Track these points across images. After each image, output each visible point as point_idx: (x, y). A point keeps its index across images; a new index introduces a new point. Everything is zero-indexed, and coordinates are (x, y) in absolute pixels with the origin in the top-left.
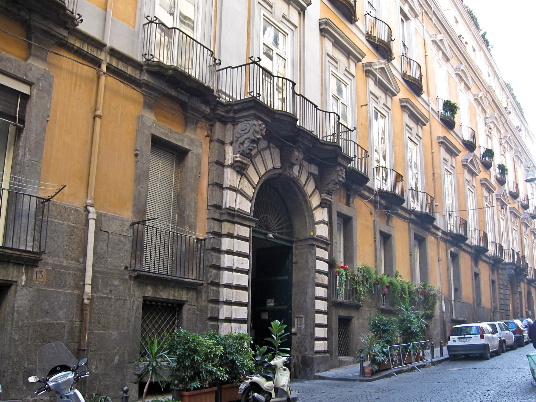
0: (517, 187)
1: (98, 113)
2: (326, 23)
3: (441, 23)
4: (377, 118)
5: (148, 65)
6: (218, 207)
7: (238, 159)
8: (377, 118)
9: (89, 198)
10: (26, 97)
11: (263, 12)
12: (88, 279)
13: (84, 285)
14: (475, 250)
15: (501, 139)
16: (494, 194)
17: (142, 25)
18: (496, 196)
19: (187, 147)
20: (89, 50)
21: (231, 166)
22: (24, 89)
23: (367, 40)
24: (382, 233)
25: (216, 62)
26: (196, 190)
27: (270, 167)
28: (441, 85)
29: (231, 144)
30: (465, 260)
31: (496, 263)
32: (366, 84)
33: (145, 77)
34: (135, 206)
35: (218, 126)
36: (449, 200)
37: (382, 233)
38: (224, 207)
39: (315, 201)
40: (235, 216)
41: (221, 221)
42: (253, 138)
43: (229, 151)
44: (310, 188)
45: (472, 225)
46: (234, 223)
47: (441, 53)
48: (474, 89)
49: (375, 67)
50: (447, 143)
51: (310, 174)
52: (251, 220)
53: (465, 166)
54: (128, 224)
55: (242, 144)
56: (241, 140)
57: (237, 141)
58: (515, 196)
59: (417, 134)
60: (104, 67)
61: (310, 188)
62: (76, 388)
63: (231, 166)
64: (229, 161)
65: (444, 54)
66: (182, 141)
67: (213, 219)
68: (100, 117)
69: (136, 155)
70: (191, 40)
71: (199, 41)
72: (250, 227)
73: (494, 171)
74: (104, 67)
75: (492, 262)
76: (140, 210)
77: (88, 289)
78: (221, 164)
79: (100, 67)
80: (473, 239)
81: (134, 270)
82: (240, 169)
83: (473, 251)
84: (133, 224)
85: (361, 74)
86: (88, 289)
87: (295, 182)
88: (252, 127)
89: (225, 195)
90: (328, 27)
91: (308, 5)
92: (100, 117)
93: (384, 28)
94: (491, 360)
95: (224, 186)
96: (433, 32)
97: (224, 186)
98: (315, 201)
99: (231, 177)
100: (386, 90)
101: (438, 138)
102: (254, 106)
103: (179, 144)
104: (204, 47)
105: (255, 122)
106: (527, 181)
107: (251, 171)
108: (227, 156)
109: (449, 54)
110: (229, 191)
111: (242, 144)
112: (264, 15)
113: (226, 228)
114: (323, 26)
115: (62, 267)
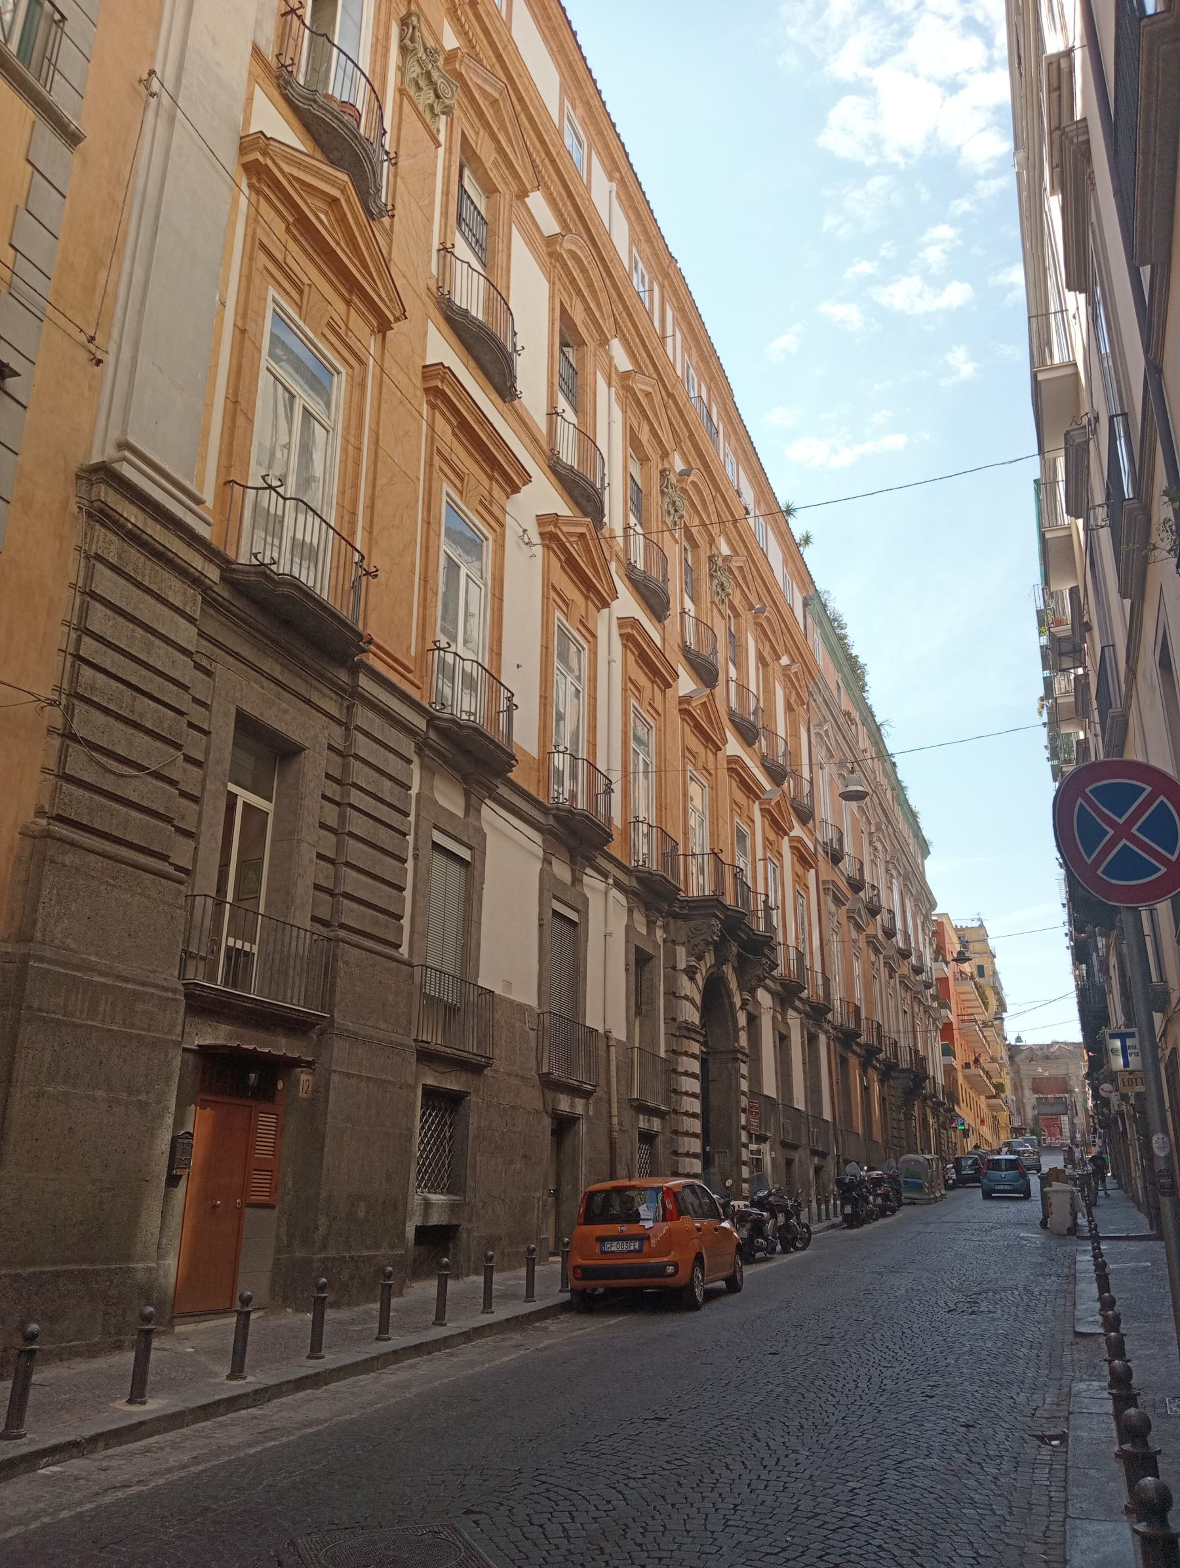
0: (861, 870)
14: (866, 1050)
15: (887, 862)
16: (881, 956)
18: (620, 626)
23: (549, 467)
24: (639, 951)
31: (888, 1071)
37: (639, 951)
45: (837, 994)
47: (824, 748)
49: (565, 529)
50: (512, 475)
58: (905, 954)
59: (650, 704)
62: (901, 1155)
70: (324, 525)
71: (358, 547)
75: (883, 1067)
80: (837, 1016)
83: (863, 1053)
91: (397, 319)
94: (706, 1309)
100: (707, 739)
104: (329, 525)
106: (848, 796)
107: (698, 977)
112: (274, 301)
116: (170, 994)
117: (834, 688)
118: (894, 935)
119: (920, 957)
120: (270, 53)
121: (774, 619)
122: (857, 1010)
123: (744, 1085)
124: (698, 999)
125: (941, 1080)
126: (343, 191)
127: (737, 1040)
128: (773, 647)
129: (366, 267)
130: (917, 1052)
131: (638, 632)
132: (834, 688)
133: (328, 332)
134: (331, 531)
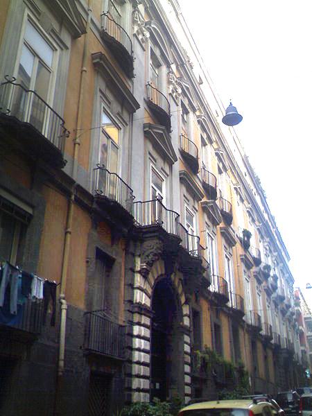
1: (69, 230)
2: (184, 174)
3: (239, 177)
4: (22, 82)
5: (98, 198)
6: (131, 302)
7: (145, 267)
8: (22, 82)
9: (62, 292)
10: (31, 217)
11: (151, 164)
12: (62, 356)
13: (59, 360)
17: (92, 169)
19: (114, 257)
20: (67, 187)
21: (139, 272)
22: (30, 211)
25: (132, 197)
26: (118, 288)
27: (160, 273)
28: (241, 222)
29: (139, 256)
30: (259, 345)
32: (203, 217)
33: (95, 206)
34: (86, 300)
35: (131, 243)
36: (249, 307)
38: (134, 302)
39: (183, 300)
40: (141, 309)
41: (133, 313)
42: (155, 252)
43: (138, 261)
44: (180, 290)
46: (141, 314)
48: (257, 222)
51: (180, 279)
52: (151, 312)
53: (255, 276)
54: (82, 314)
55: (148, 256)
56: (146, 254)
57: (143, 254)
60: (73, 197)
61: (180, 290)
63: (139, 272)
64: (138, 269)
65: (241, 197)
66: (112, 253)
67: (128, 311)
68: (70, 233)
69: (87, 262)
72: (149, 317)
73: (270, 279)
74: (73, 197)
76: (89, 303)
77: (62, 363)
78: (133, 270)
79: (70, 197)
81: (87, 349)
82: (145, 274)
84: (86, 313)
85: (200, 210)
86: (62, 363)
87: (172, 284)
88: (152, 245)
89: (135, 293)
90: (102, 62)
92: (70, 233)
93: (211, 176)
95: (135, 286)
96: (235, 182)
97: (135, 286)
98: (183, 300)
99: (138, 280)
101: (241, 256)
102: (157, 230)
103: (110, 254)
104: (49, 107)
105: (158, 241)
107: (150, 276)
108: (137, 265)
109: (244, 198)
110: (138, 291)
111: (148, 256)
113: (136, 318)
114: (182, 176)
115: (46, 345)
116: (293, 382)
117: (244, 174)
118: (277, 288)
119: (289, 301)
120: (146, 98)
121: (224, 153)
122: (259, 318)
123: (187, 348)
124: (150, 291)
125: (300, 355)
126: (164, 132)
127: (182, 321)
128: (223, 163)
129: (67, 7)
130: (289, 341)
131: (104, 62)
132: (244, 174)
133: (52, 34)
134: (50, 110)
